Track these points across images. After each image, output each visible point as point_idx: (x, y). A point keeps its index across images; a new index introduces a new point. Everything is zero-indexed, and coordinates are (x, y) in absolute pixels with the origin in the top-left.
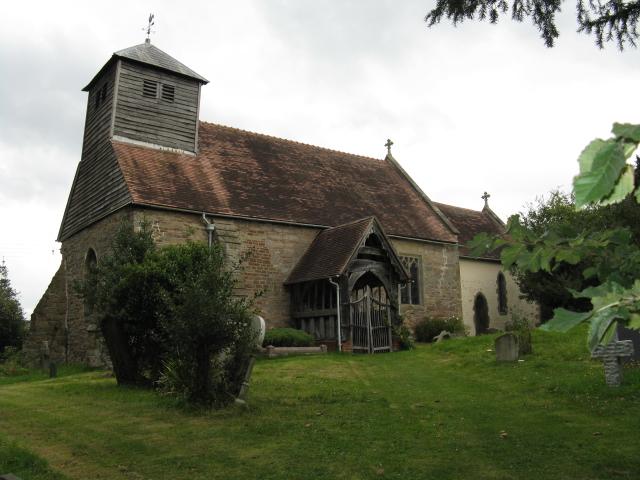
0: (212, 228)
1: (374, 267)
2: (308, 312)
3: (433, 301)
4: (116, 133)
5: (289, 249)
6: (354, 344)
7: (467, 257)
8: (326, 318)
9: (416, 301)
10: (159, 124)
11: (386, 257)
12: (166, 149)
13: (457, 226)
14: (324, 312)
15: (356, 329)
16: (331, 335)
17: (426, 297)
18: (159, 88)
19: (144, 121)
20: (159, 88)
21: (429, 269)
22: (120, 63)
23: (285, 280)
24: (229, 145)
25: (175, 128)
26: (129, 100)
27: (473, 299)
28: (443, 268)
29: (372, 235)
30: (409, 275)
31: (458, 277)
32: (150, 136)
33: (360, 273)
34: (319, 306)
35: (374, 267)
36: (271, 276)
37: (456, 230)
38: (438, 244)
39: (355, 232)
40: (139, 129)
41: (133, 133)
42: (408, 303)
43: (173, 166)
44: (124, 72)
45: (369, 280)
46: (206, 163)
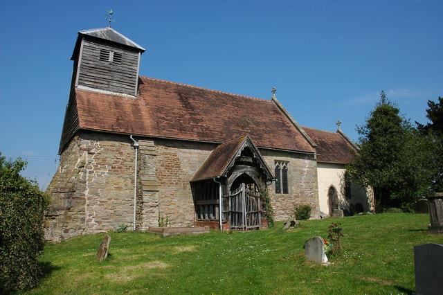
0: (138, 145)
1: (248, 170)
2: (204, 202)
3: (298, 191)
4: (79, 84)
5: (269, 157)
6: (232, 224)
7: (322, 163)
8: (209, 206)
9: (286, 191)
10: (110, 78)
11: (257, 164)
12: (115, 94)
13: (316, 142)
14: (209, 202)
15: (233, 213)
16: (217, 218)
17: (292, 188)
18: (111, 55)
19: (100, 76)
20: (111, 55)
21: (296, 171)
22: (83, 38)
23: (191, 179)
24: (161, 91)
25: (122, 80)
26: (90, 62)
27: (327, 189)
28: (305, 170)
29: (246, 148)
30: (274, 175)
31: (316, 176)
32: (104, 86)
33: (237, 174)
34: (210, 198)
35: (248, 170)
36: (181, 177)
37: (314, 144)
38: (302, 155)
39: (236, 145)
40: (96, 81)
41: (92, 84)
42: (280, 192)
43: (117, 104)
44: (87, 44)
45: (245, 179)
46: (142, 102)
